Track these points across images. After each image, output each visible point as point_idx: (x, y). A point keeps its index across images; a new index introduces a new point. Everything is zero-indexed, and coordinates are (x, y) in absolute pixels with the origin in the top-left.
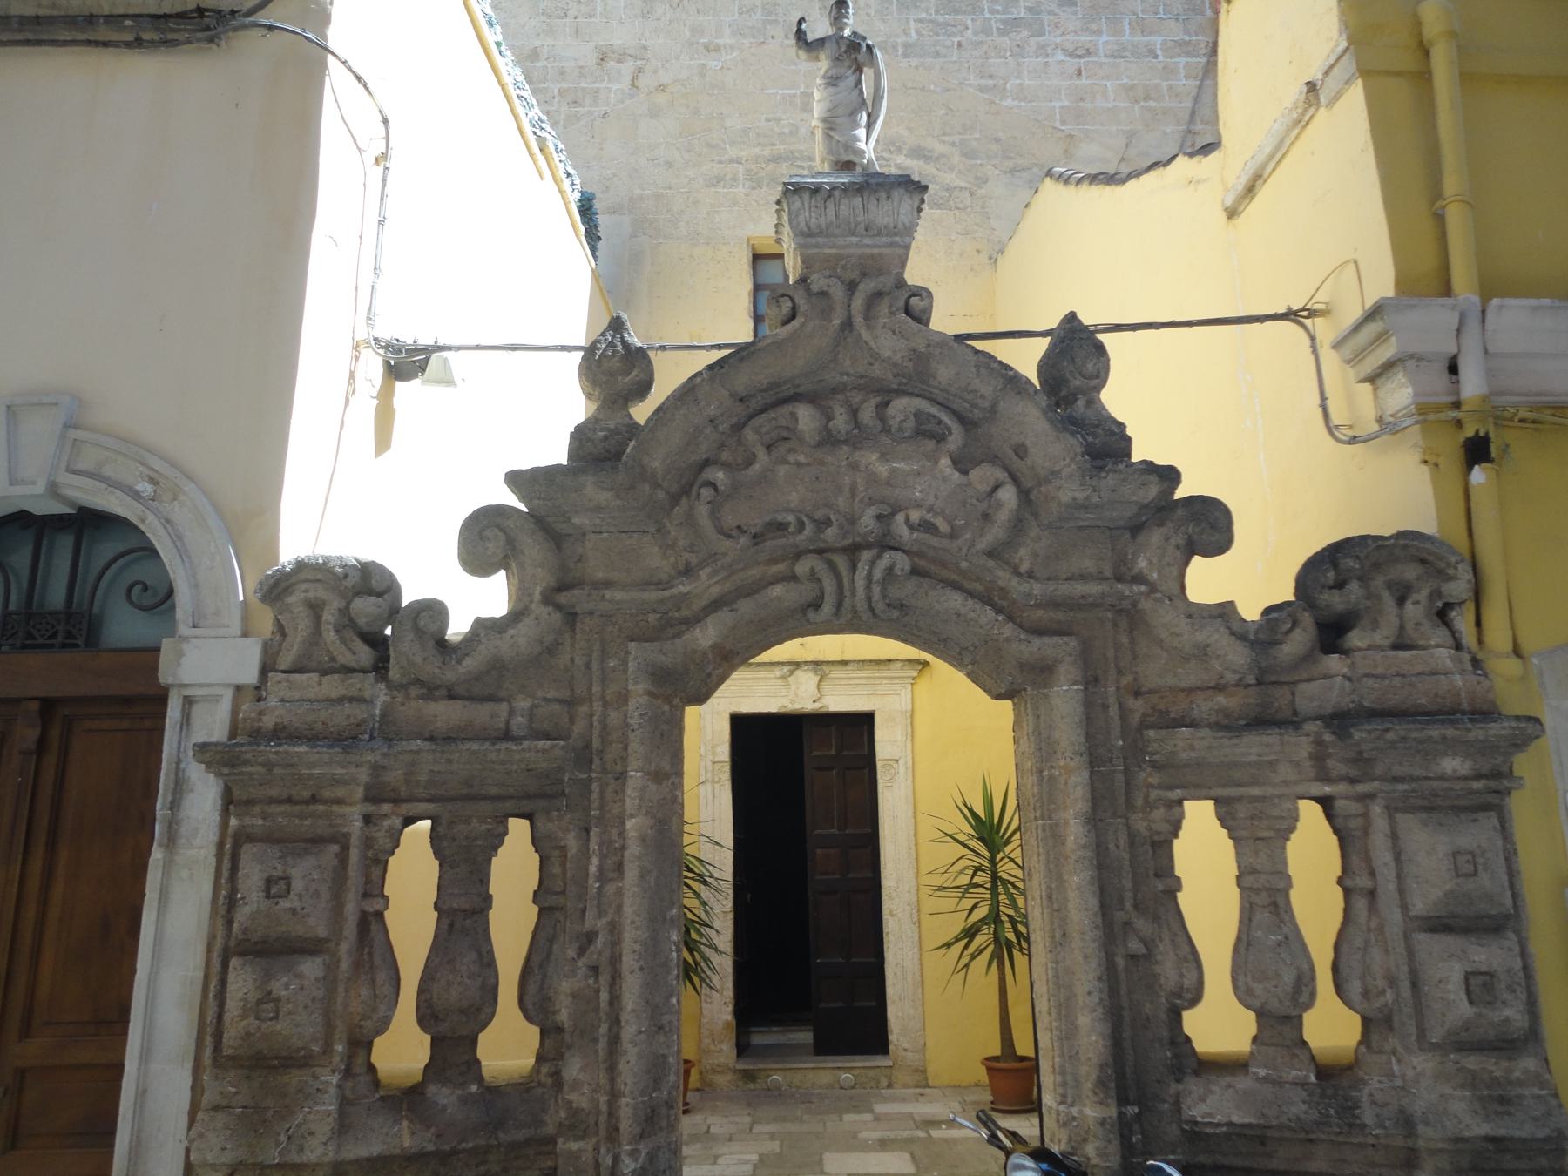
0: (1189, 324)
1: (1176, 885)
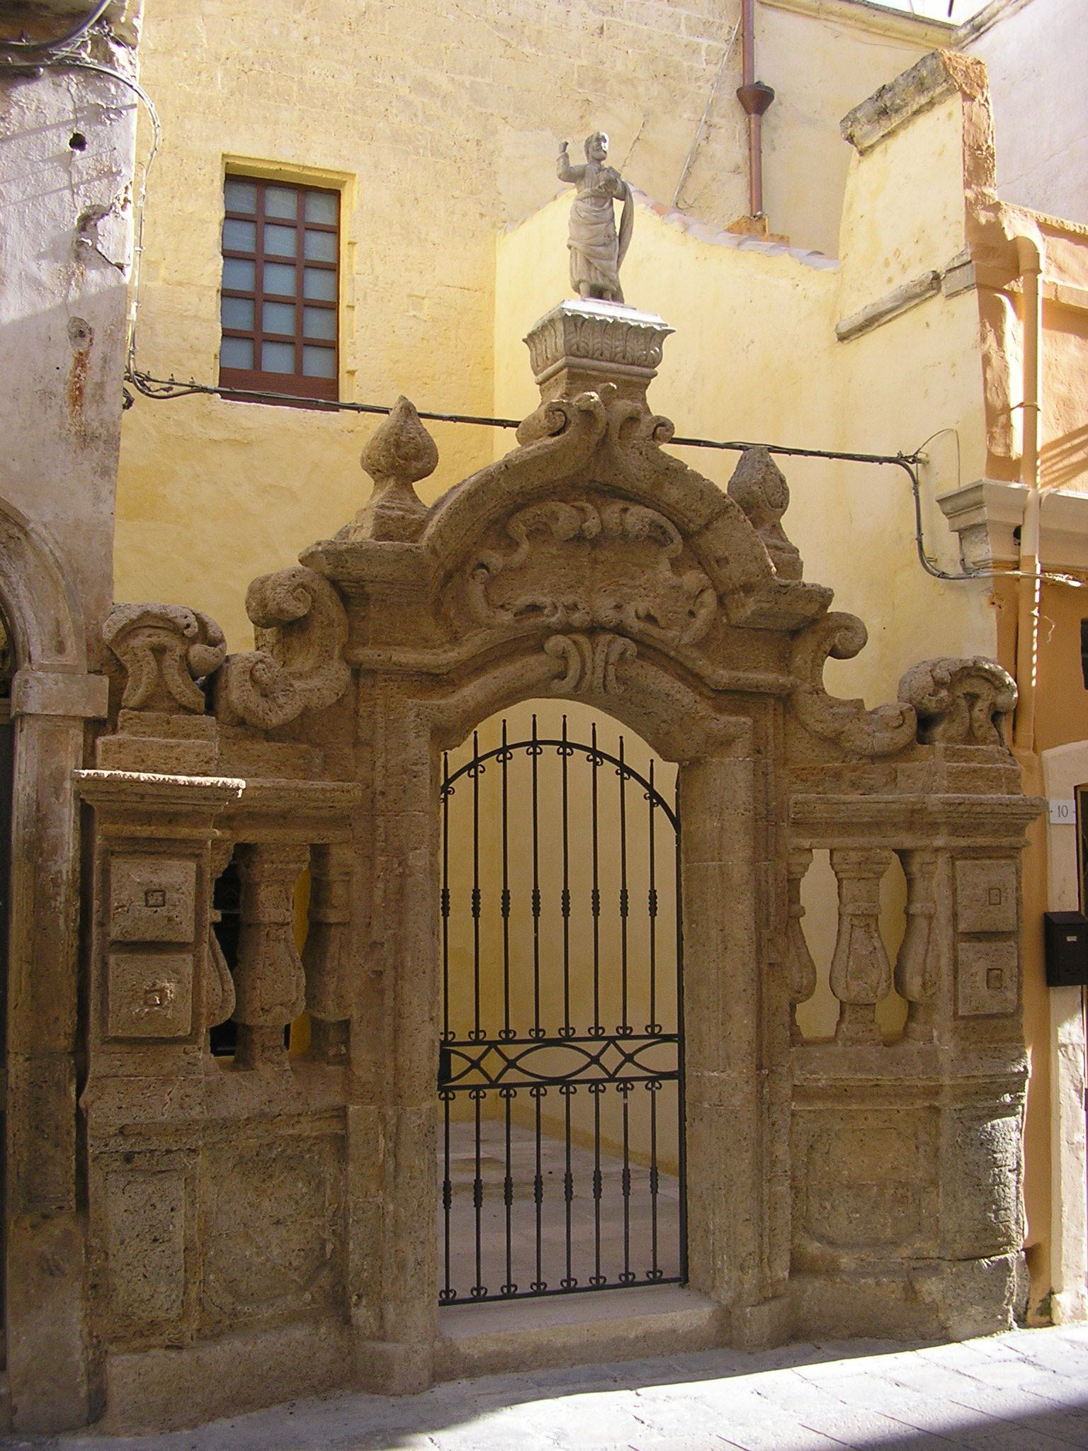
0: (830, 456)
1: (802, 912)
